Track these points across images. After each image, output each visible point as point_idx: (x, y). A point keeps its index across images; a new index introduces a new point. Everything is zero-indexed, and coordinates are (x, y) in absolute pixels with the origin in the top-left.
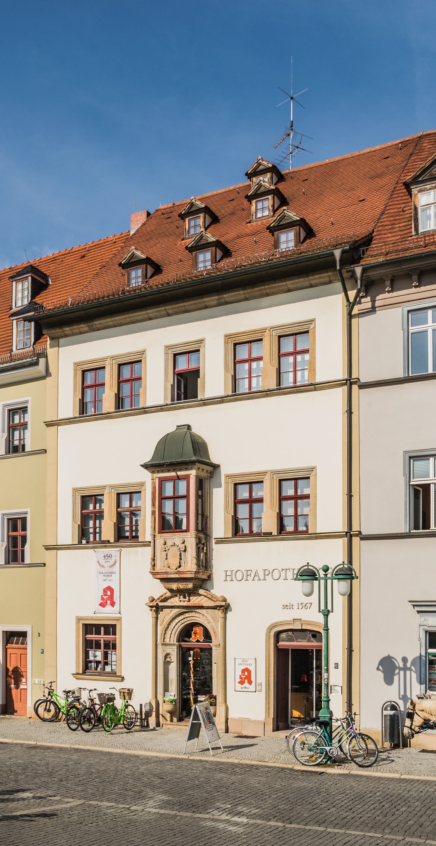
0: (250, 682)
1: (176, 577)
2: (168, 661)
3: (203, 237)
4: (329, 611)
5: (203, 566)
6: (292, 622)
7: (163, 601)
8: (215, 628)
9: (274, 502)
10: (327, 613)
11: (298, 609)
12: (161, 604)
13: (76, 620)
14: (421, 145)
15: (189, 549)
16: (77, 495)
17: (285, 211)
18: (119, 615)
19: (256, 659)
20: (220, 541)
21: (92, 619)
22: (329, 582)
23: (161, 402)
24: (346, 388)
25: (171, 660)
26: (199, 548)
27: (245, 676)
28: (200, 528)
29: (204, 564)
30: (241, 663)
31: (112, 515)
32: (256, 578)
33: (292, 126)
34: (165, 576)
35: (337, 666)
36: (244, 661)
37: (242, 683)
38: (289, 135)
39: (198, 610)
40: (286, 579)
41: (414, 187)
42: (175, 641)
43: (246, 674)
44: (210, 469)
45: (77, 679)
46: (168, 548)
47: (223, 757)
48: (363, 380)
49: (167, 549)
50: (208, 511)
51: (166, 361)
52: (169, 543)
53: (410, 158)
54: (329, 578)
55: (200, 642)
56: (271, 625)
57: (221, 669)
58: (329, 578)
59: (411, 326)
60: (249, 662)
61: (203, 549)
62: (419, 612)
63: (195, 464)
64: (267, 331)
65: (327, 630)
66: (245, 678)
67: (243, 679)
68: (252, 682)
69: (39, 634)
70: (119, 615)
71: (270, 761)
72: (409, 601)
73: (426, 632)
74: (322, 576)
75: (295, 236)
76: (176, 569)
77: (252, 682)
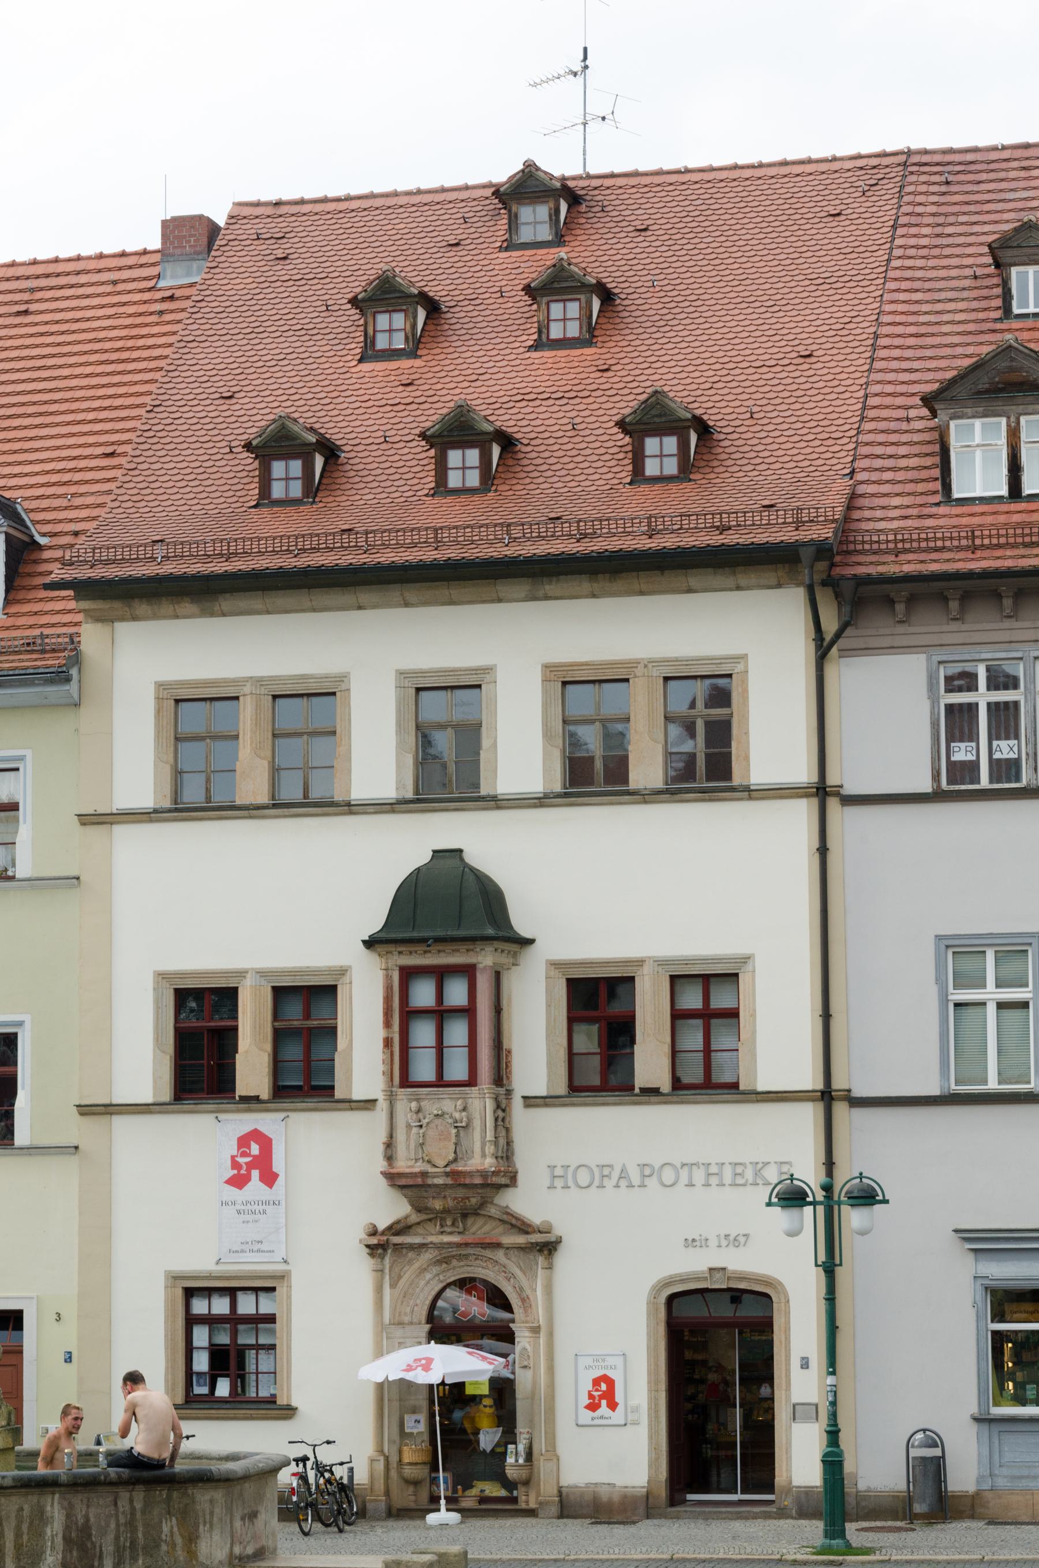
6: (707, 1275)
11: (719, 1246)
20: (530, 1102)
30: (591, 1364)
36: (598, 1361)
37: (593, 1407)
39: (488, 1253)
40: (691, 1185)
41: (942, 406)
43: (604, 1387)
48: (850, 789)
56: (659, 1282)
60: (610, 1361)
66: (601, 1397)
68: (617, 1404)
69: (59, 1314)
70: (283, 1267)
73: (986, 1288)
77: (617, 1404)
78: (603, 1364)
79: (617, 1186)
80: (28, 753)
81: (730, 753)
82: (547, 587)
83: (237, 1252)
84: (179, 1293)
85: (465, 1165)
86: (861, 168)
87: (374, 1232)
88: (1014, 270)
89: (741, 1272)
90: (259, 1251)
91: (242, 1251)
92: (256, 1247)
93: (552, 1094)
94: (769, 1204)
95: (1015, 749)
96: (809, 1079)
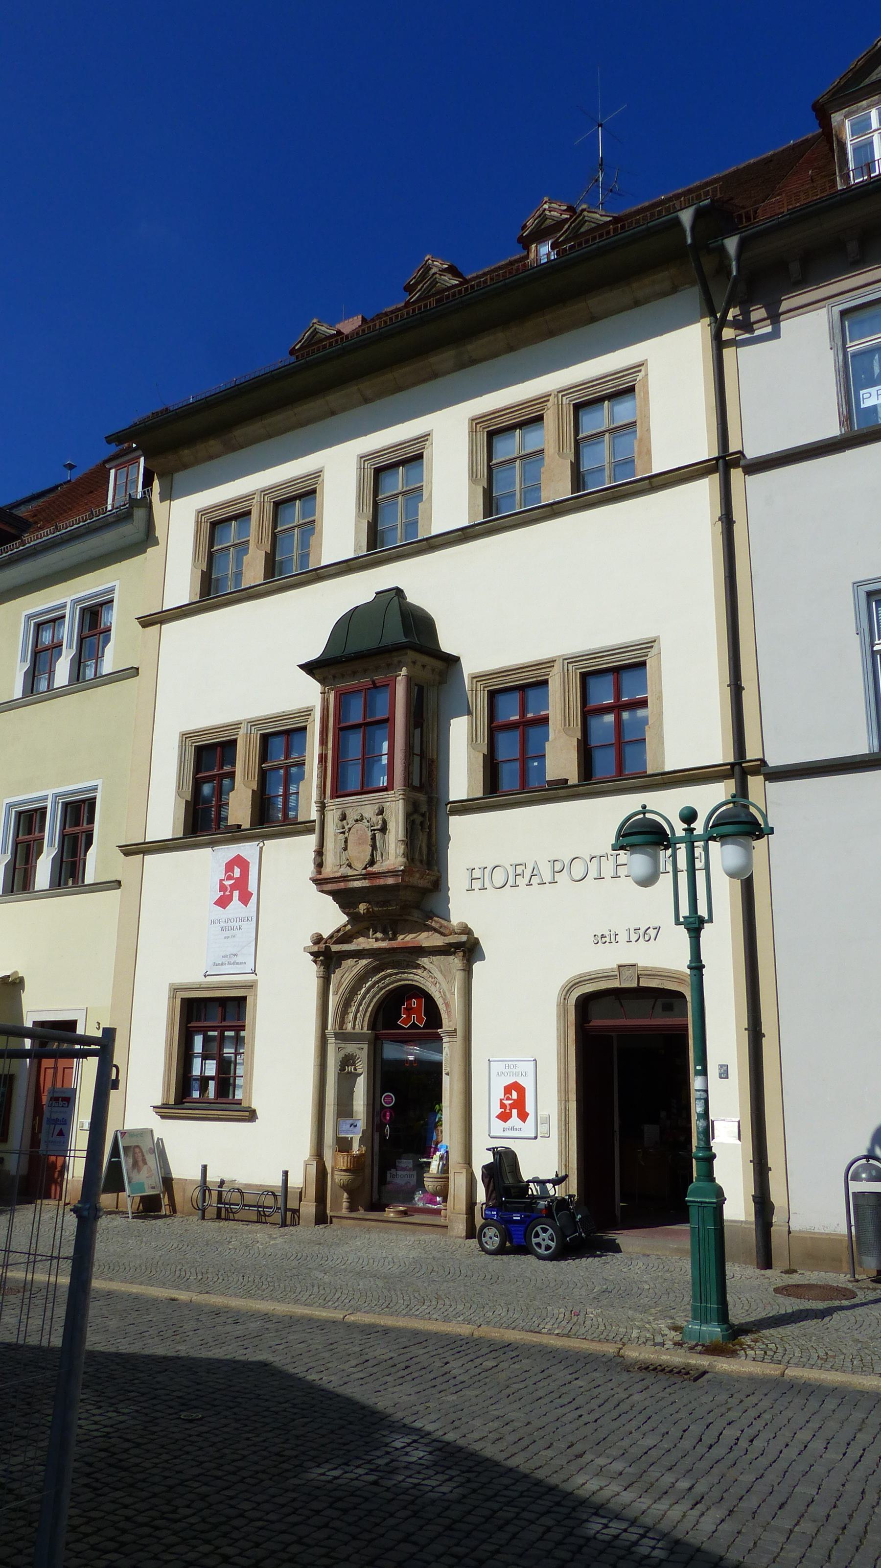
0: (523, 1116)
1: (364, 885)
2: (348, 1073)
3: (437, 282)
4: (701, 921)
5: (421, 861)
6: (617, 973)
7: (340, 941)
8: (448, 995)
9: (572, 719)
10: (696, 926)
12: (335, 948)
13: (170, 990)
15: (391, 826)
16: (187, 744)
17: (585, 213)
18: (253, 977)
19: (535, 1060)
21: (199, 988)
23: (463, 521)
24: (716, 477)
25: (355, 1069)
26: (413, 822)
27: (511, 1102)
28: (416, 783)
29: (425, 857)
31: (250, 776)
32: (535, 880)
34: (342, 885)
36: (509, 1067)
37: (504, 1117)
42: (365, 1028)
43: (515, 1095)
44: (439, 664)
45: (163, 1117)
46: (349, 826)
47: (434, 1316)
49: (347, 827)
50: (435, 749)
51: (360, 481)
52: (352, 815)
54: (699, 838)
55: (420, 1028)
56: (569, 982)
57: (458, 1086)
59: (850, 342)
61: (422, 824)
63: (406, 654)
64: (551, 398)
66: (512, 1106)
67: (508, 1107)
68: (528, 1114)
71: (556, 1332)
76: (365, 868)
77: (528, 1114)
78: (514, 1070)
79: (529, 885)
80: (117, 583)
82: (470, 347)
83: (219, 964)
85: (381, 866)
87: (318, 939)
90: (235, 963)
91: (223, 964)
92: (234, 959)
93: (471, 797)
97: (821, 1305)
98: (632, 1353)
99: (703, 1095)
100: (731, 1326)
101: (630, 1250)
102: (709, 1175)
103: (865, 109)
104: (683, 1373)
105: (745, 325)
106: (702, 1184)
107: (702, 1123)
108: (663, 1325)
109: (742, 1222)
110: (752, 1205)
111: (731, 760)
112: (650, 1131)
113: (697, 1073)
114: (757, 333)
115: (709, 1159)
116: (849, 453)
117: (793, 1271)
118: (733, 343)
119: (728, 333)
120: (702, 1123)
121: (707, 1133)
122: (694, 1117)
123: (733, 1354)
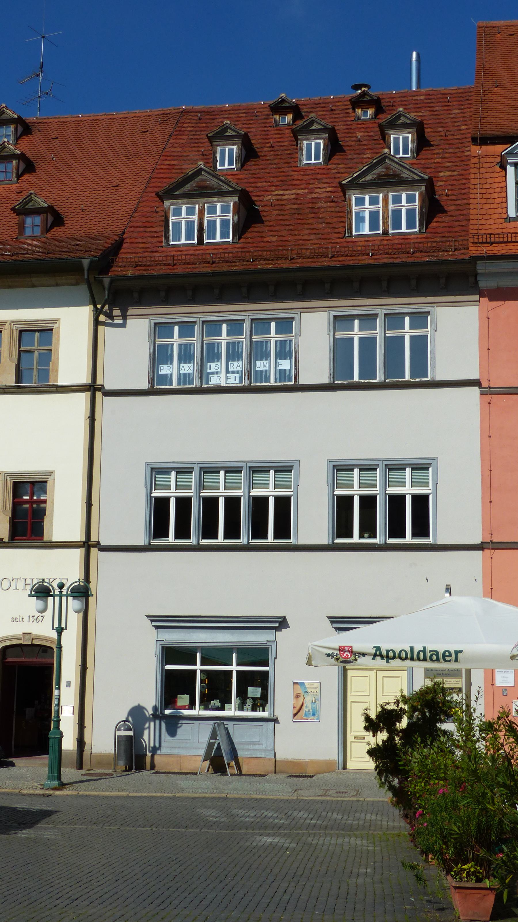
4: (62, 629)
6: (22, 637)
14: (182, 124)
17: (32, 195)
22: (64, 598)
33: (42, 67)
35: (69, 685)
38: (38, 75)
53: (169, 140)
54: (64, 595)
58: (64, 595)
62: (157, 627)
64: (7, 324)
65: (60, 648)
72: (148, 616)
74: (57, 592)
75: (42, 222)
81: (49, 369)
84: (153, 325)
86: (162, 114)
88: (219, 148)
89: (39, 636)
94: (30, 595)
95: (192, 368)
96: (78, 536)
97: (98, 778)
98: (25, 792)
99: (58, 697)
100: (62, 782)
101: (20, 765)
102: (58, 727)
103: (180, 204)
104: (44, 795)
105: (111, 316)
106: (55, 730)
107: (57, 708)
108: (36, 784)
109: (71, 750)
110: (76, 742)
111: (84, 540)
112: (29, 712)
113: (56, 689)
114: (116, 321)
115: (58, 721)
116: (151, 397)
117: (92, 770)
118: (104, 324)
119: (102, 318)
120: (57, 708)
121: (58, 712)
122: (53, 705)
123: (62, 790)
